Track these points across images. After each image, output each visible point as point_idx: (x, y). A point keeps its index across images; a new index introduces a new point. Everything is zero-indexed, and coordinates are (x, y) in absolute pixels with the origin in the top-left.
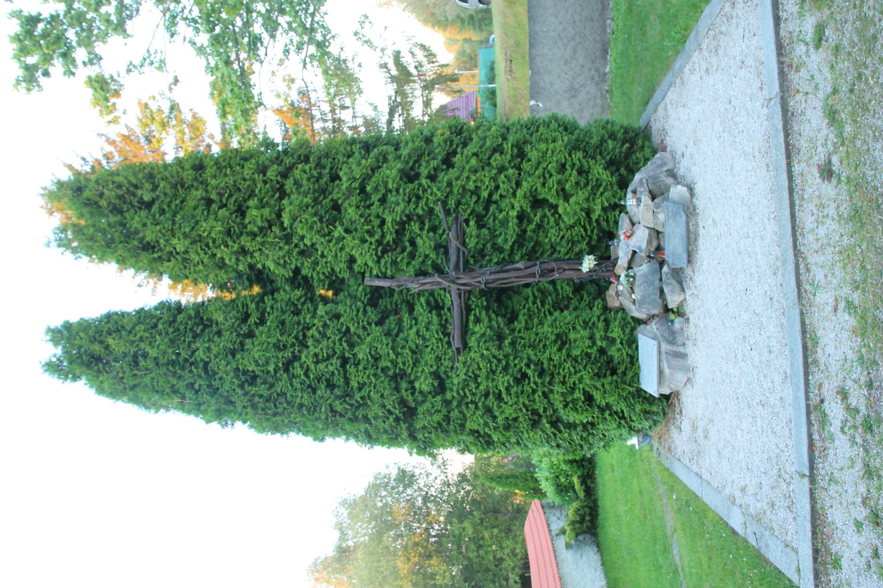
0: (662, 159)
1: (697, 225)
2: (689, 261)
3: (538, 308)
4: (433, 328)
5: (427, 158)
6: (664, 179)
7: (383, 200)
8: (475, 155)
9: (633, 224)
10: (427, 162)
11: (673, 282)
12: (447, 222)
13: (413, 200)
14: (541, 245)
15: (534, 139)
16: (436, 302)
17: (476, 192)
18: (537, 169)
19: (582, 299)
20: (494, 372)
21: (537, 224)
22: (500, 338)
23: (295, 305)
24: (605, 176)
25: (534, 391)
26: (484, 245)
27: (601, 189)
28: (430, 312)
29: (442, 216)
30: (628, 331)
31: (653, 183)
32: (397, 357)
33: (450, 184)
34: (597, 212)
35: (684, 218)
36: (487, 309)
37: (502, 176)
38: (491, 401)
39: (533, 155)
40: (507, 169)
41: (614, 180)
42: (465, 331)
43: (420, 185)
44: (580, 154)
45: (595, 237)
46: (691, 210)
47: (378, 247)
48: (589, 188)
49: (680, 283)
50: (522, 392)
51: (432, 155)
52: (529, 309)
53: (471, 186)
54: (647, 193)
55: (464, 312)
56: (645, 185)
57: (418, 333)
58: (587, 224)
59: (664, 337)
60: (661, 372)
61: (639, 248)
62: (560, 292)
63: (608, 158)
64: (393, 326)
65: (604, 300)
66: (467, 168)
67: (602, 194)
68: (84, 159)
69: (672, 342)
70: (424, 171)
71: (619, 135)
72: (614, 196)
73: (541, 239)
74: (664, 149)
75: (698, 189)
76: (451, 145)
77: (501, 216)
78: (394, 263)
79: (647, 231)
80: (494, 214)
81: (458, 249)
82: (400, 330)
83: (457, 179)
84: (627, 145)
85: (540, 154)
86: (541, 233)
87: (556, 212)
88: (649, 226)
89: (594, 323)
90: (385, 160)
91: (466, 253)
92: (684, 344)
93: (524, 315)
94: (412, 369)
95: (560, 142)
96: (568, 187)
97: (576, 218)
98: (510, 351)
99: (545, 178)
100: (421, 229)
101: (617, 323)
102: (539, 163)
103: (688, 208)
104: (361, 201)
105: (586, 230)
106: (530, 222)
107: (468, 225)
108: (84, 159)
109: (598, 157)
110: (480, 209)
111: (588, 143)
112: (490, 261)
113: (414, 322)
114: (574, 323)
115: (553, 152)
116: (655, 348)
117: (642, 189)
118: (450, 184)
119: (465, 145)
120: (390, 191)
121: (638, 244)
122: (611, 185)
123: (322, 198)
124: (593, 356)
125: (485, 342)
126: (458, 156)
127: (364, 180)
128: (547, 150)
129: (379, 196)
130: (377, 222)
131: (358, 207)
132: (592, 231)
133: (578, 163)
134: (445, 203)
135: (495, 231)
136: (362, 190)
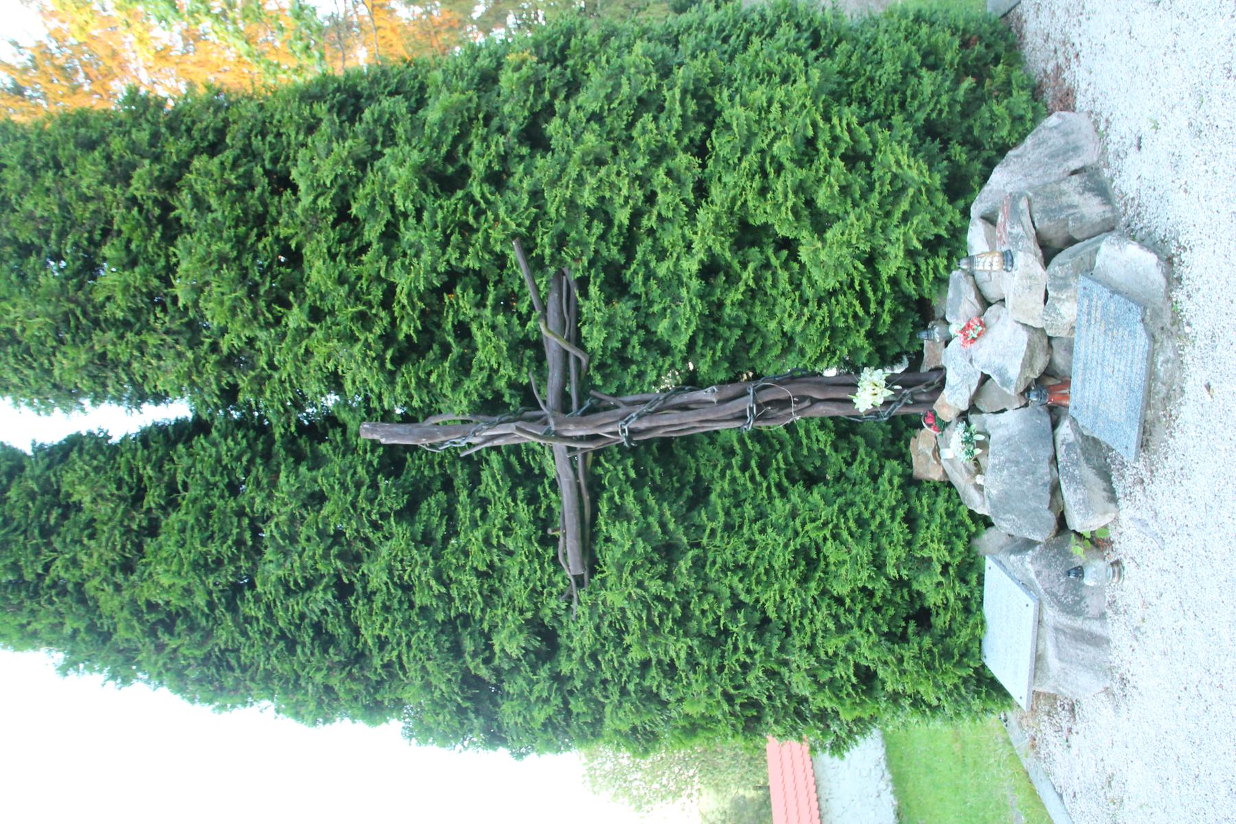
0: (1066, 134)
1: (1179, 362)
2: (1144, 445)
3: (752, 478)
4: (521, 532)
5: (482, 131)
6: (1076, 199)
7: (390, 235)
8: (596, 117)
9: (986, 303)
10: (484, 139)
11: (1088, 473)
12: (537, 288)
13: (455, 238)
14: (758, 331)
15: (736, 69)
16: (528, 468)
17: (601, 212)
18: (744, 151)
19: (854, 454)
20: (656, 630)
21: (749, 289)
22: (669, 551)
23: (230, 472)
24: (915, 172)
25: (745, 667)
26: (625, 342)
27: (904, 205)
28: (512, 493)
29: (523, 273)
30: (960, 546)
31: (1046, 211)
32: (447, 586)
33: (536, 195)
34: (893, 263)
35: (1142, 340)
36: (636, 485)
37: (661, 171)
38: (654, 679)
39: (735, 114)
40: (672, 153)
41: (937, 180)
42: (589, 536)
43: (470, 198)
44: (850, 114)
45: (887, 318)
46: (1167, 320)
47: (384, 351)
48: (875, 198)
49: (1105, 474)
50: (721, 668)
51: (495, 122)
52: (733, 480)
53: (588, 198)
54: (1032, 245)
55: (586, 498)
56: (1026, 219)
57: (487, 540)
58: (868, 288)
59: (1053, 595)
60: (1038, 659)
61: (1001, 373)
62: (805, 441)
63: (921, 117)
64: (435, 520)
65: (904, 458)
66: (577, 154)
67: (905, 218)
68: (15, 44)
69: (1073, 608)
70: (478, 167)
71: (948, 57)
72: (935, 222)
73: (757, 320)
74: (1066, 101)
75: (1195, 265)
76: (539, 92)
77: (662, 269)
78: (423, 384)
79: (1023, 336)
80: (646, 264)
81: (566, 354)
82: (452, 532)
83: (554, 183)
84: (968, 82)
85: (754, 116)
86: (757, 309)
87: (794, 256)
88: (1030, 323)
89: (882, 525)
90: (391, 140)
91: (584, 361)
92: (1103, 616)
93: (722, 495)
94: (483, 610)
95: (801, 84)
96: (821, 200)
97: (843, 277)
98: (692, 584)
99: (765, 175)
100: (481, 304)
101: (935, 529)
102: (751, 136)
103: (1156, 314)
104: (340, 242)
105: (865, 303)
106: (732, 280)
107: (585, 294)
108: (15, 44)
109: (897, 119)
110: (614, 253)
111: (871, 80)
112: (641, 375)
113: (478, 512)
114: (836, 526)
115: (784, 108)
116: (1030, 613)
117: (1017, 230)
118: (536, 195)
119: (573, 87)
120: (405, 215)
121: (997, 361)
122: (928, 191)
123: (253, 238)
124: (879, 594)
125: (635, 568)
126: (556, 121)
127: (344, 188)
128: (770, 102)
129: (380, 228)
130: (377, 293)
131: (333, 257)
132: (881, 303)
133: (846, 137)
134: (528, 244)
135: (651, 303)
136: (342, 213)
